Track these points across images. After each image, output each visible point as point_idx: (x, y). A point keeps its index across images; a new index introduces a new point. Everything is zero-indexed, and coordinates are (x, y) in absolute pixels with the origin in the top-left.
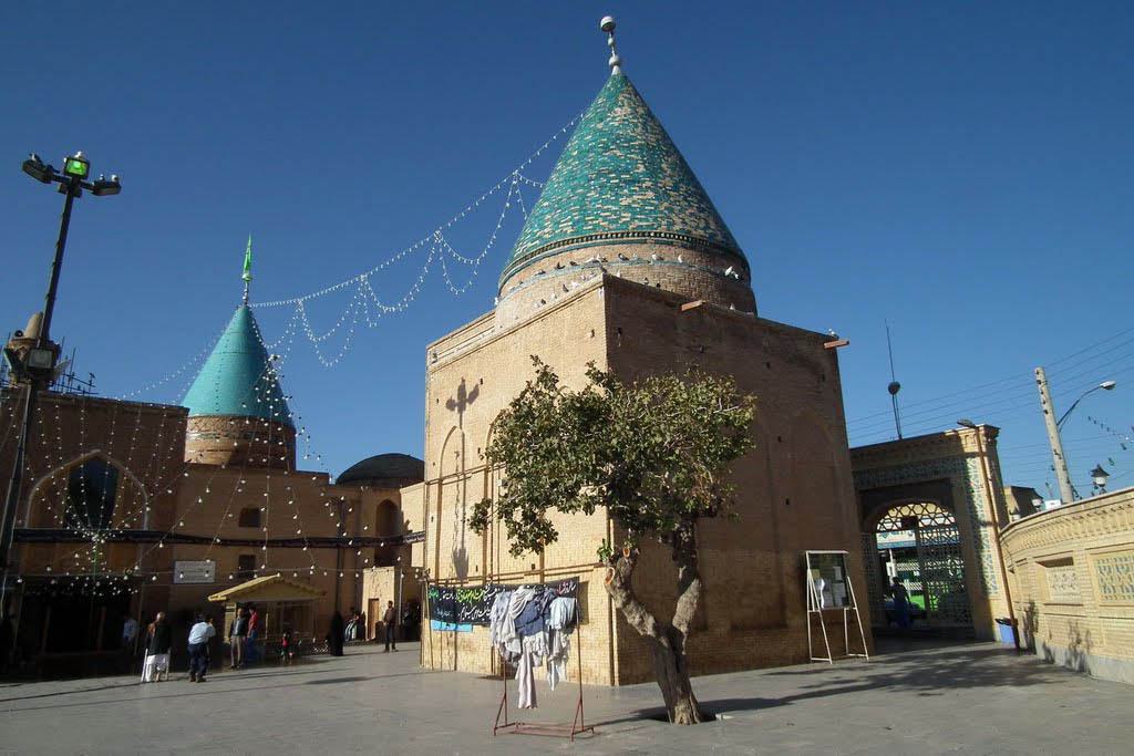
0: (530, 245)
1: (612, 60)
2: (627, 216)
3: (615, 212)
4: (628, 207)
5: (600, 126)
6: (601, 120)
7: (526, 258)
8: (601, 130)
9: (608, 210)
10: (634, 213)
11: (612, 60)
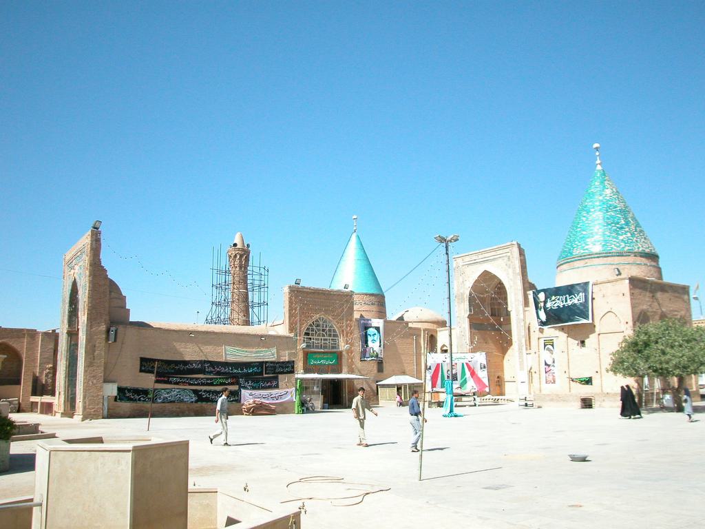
0: (582, 251)
1: (598, 162)
2: (623, 245)
3: (618, 242)
4: (622, 240)
5: (601, 198)
6: (601, 195)
7: (581, 256)
8: (602, 201)
9: (614, 241)
10: (625, 243)
11: (598, 162)
